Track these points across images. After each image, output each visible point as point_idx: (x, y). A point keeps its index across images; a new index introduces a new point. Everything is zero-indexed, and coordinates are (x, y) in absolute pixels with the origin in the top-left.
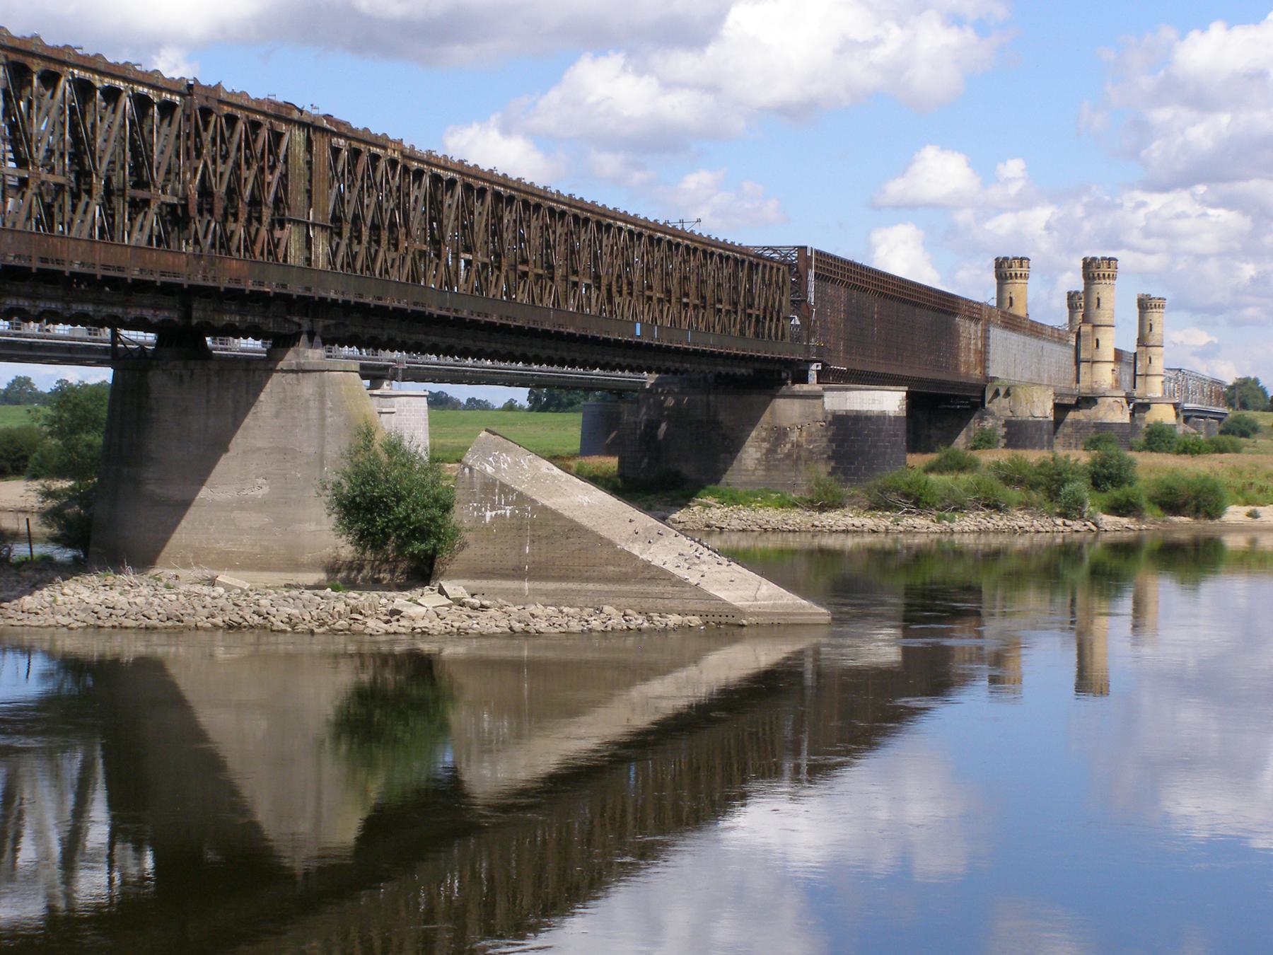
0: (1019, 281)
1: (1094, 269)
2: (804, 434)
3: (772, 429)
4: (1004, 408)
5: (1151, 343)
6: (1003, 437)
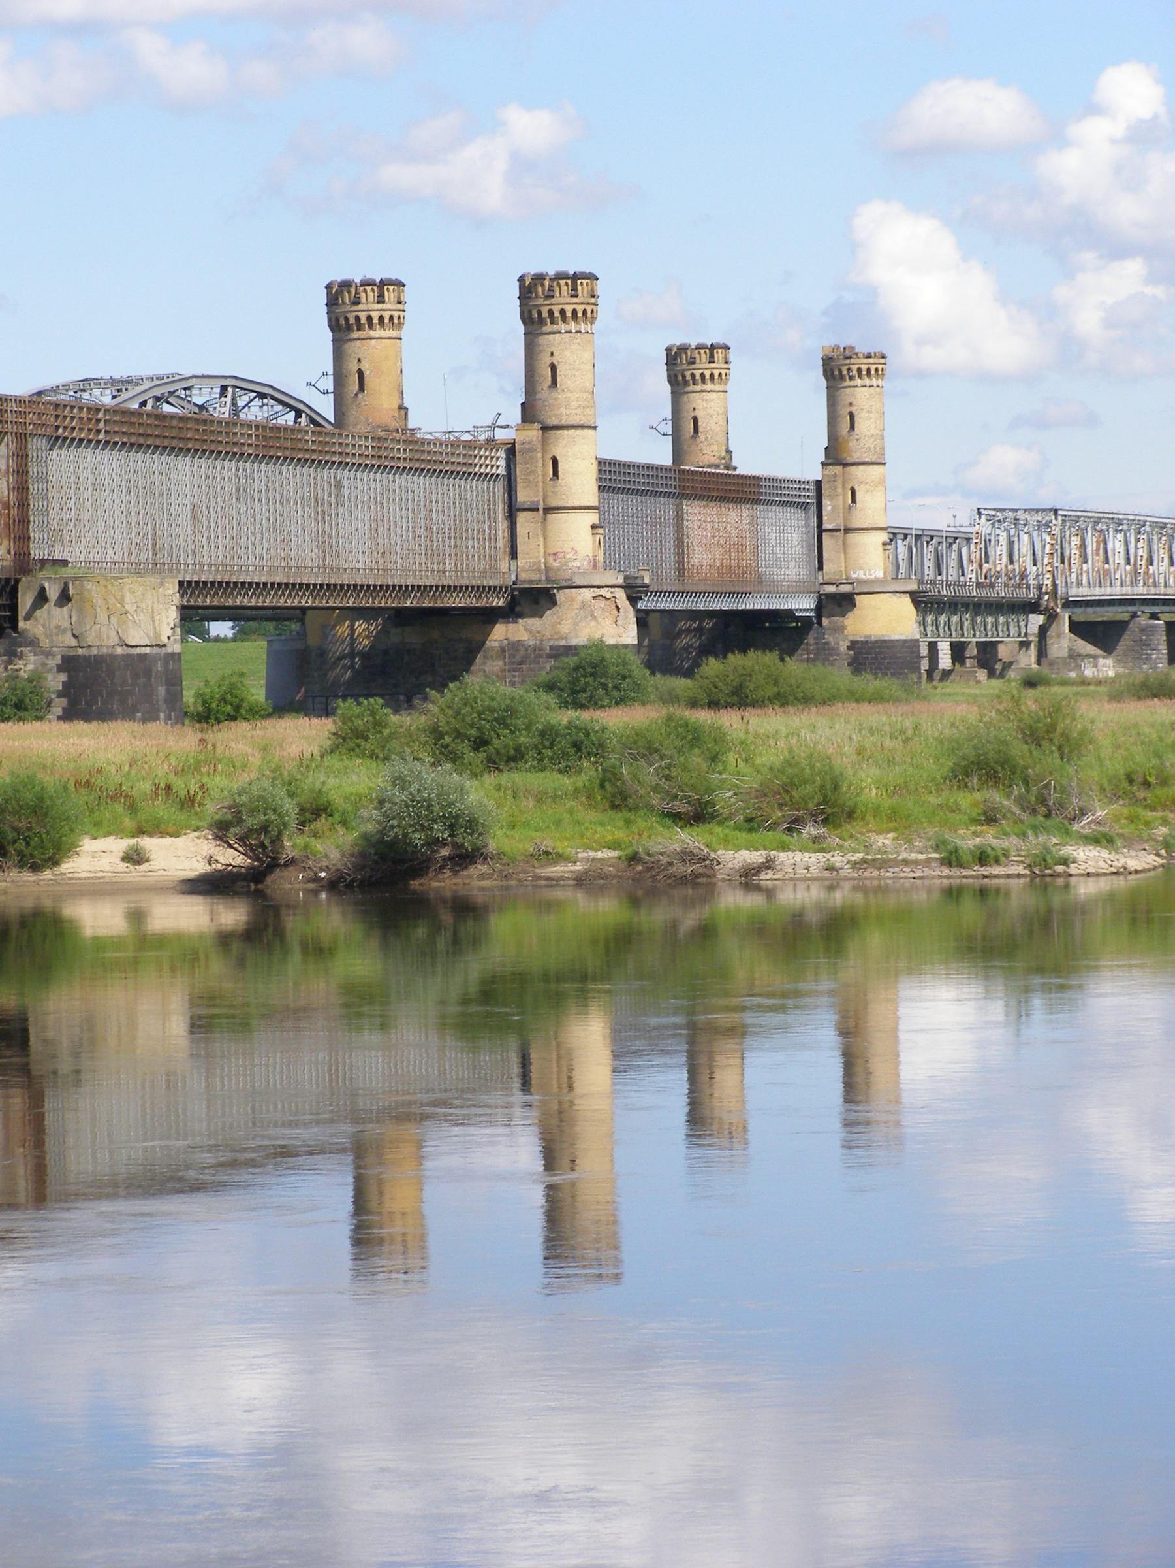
0: (378, 332)
1: (540, 301)
4: (60, 630)
5: (855, 457)
6: (60, 694)
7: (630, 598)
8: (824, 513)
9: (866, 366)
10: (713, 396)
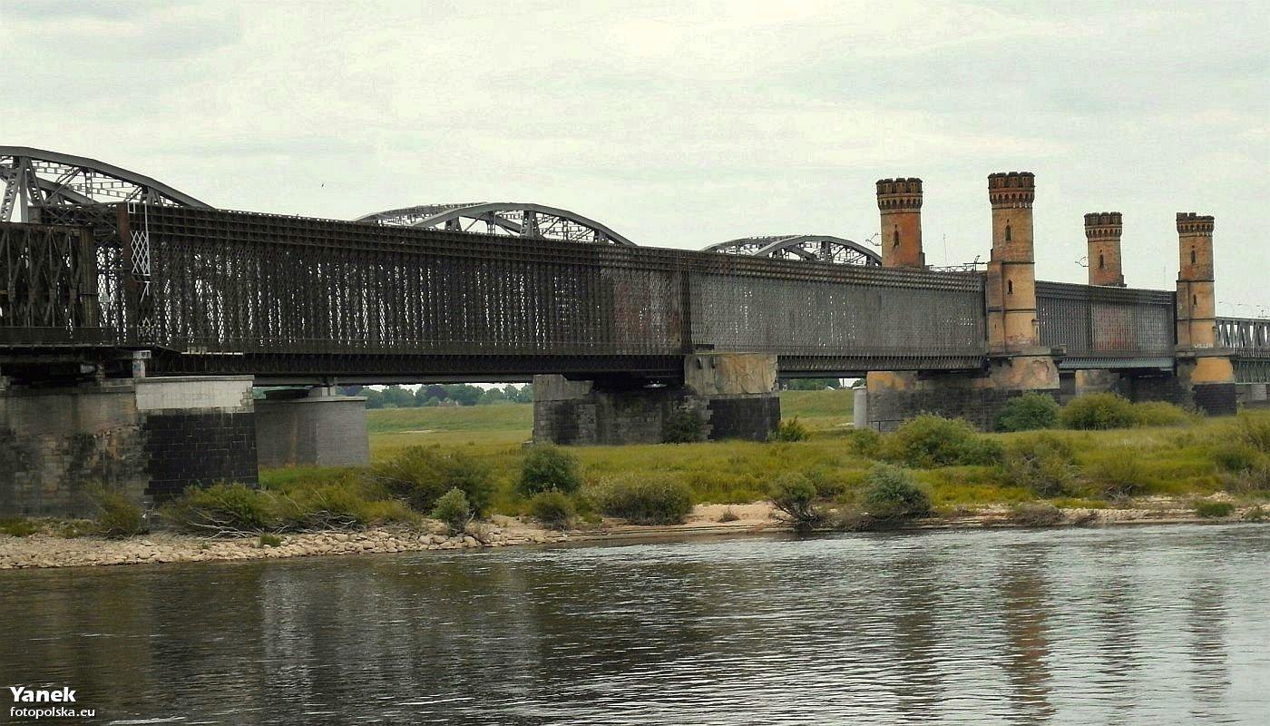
2: (114, 442)
3: (76, 438)
7: (1055, 362)
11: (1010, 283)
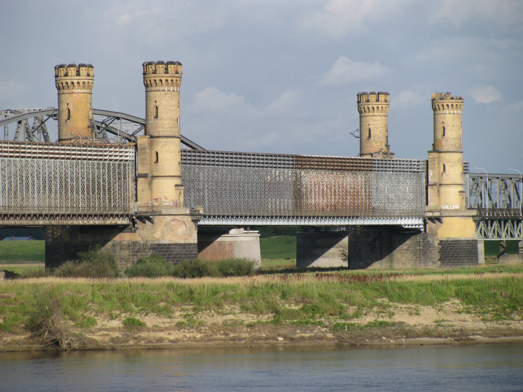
5: (445, 149)
7: (193, 221)
8: (429, 177)
9: (456, 104)
10: (378, 118)
11: (157, 154)
